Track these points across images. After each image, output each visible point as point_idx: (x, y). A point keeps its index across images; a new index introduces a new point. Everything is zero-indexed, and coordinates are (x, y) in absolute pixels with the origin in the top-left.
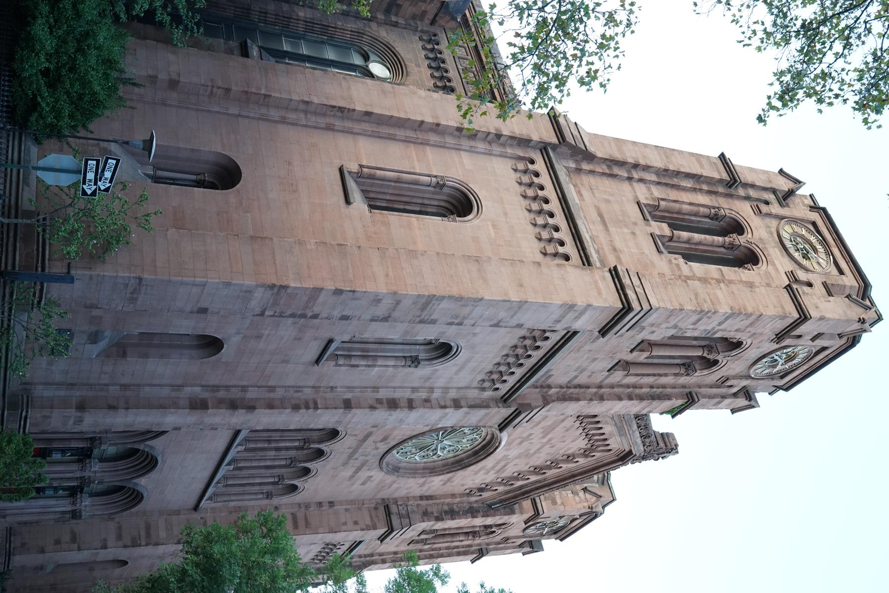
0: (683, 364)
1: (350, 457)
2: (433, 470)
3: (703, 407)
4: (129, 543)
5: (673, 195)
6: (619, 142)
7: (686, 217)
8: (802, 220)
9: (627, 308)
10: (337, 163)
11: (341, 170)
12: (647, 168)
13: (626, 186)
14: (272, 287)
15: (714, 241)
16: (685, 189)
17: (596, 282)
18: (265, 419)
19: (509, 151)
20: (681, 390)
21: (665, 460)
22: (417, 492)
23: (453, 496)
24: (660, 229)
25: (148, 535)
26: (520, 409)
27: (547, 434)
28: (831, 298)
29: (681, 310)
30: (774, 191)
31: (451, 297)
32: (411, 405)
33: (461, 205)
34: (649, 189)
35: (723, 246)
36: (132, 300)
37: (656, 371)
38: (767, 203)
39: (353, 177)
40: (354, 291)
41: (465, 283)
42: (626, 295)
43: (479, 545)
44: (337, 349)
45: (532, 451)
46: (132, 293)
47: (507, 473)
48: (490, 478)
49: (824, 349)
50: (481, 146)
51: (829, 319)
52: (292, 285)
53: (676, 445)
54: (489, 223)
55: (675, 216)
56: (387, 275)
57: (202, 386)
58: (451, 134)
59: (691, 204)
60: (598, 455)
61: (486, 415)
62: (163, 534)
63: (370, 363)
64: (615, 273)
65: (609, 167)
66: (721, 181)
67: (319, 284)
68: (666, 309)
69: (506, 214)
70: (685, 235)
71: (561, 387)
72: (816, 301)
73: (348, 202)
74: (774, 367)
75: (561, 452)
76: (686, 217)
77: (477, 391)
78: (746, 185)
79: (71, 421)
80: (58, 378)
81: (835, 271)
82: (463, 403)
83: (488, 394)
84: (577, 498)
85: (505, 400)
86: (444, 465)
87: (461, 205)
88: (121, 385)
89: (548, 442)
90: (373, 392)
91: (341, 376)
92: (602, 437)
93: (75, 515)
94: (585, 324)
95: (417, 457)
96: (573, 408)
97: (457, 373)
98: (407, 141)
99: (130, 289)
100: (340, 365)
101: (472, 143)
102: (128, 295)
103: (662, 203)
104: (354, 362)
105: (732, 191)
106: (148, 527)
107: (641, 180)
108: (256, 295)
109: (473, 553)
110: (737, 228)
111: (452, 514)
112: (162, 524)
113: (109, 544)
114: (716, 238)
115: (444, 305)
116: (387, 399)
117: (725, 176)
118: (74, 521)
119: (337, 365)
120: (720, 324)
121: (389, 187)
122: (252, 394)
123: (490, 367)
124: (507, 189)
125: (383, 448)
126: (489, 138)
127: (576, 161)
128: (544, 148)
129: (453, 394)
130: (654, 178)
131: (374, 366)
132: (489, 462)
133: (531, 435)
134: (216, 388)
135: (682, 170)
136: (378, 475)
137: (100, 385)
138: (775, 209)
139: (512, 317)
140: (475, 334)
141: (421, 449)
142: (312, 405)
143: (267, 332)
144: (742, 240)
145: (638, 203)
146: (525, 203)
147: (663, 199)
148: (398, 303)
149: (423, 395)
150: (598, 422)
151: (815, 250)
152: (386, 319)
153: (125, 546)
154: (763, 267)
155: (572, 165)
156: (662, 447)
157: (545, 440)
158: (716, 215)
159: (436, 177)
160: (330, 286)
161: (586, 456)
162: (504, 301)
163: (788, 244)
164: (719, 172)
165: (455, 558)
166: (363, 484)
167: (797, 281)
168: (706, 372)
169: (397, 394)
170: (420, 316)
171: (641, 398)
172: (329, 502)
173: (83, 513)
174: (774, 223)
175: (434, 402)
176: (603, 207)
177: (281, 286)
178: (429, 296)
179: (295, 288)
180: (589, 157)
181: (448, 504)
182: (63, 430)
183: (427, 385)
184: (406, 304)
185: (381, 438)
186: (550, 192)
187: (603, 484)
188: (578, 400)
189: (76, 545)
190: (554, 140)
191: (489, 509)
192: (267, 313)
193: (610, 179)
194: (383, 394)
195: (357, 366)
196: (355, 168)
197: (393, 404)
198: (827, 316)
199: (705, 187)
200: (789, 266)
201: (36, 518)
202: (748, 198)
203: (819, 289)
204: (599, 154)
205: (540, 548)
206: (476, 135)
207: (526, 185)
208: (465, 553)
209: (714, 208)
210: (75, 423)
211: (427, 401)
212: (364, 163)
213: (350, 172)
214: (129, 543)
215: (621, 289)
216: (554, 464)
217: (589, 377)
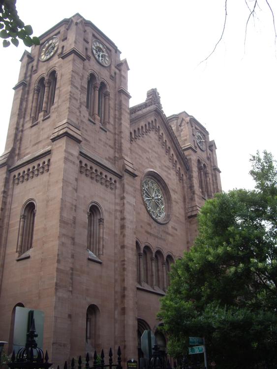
0: (105, 97)
1: (160, 238)
2: (168, 199)
3: (126, 84)
5: (29, 111)
6: (8, 137)
7: (38, 103)
8: (39, 50)
9: (66, 134)
10: (16, 261)
11: (18, 260)
12: (18, 124)
13: (26, 133)
14: (56, 289)
16: (27, 105)
17: (57, 148)
18: (131, 281)
19: (11, 186)
20: (117, 96)
21: (160, 93)
22: (181, 204)
23: (183, 187)
24: (41, 117)
27: (145, 150)
28: (68, 38)
29: (69, 108)
30: (28, 64)
31: (61, 213)
32: (123, 219)
33: (30, 207)
34: (26, 122)
35: (49, 87)
36: (65, 345)
37: (107, 109)
38: (32, 67)
39: (21, 255)
40: (58, 255)
41: (56, 205)
42: (61, 135)
43: (211, 170)
45: (157, 155)
46: (61, 346)
47: (170, 165)
48: (173, 172)
49: (94, 35)
50: (9, 200)
51: (76, 39)
52: (55, 281)
53: (153, 89)
55: (38, 109)
57: (115, 310)
58: (4, 213)
59: (32, 102)
60: (158, 125)
61: (128, 184)
63: (102, 240)
64: (54, 140)
65: (18, 141)
66: (23, 89)
67: (55, 269)
68: (69, 115)
69: (34, 188)
70: (44, 105)
71: (115, 151)
72: (70, 45)
73: (28, 257)
74: (105, 55)
75: (157, 142)
76: (38, 103)
78: (25, 77)
81: (59, 35)
82: (122, 195)
84: (184, 129)
85: (120, 177)
86: (166, 194)
87: (30, 207)
88: (115, 344)
89: (151, 150)
91: (109, 249)
92: (147, 125)
95: (163, 207)
96: (126, 145)
97: (107, 201)
98: (7, 232)
100: (103, 253)
101: (8, 203)
103: (32, 115)
107: (23, 126)
109: (215, 173)
110: (42, 80)
111: (191, 187)
114: (46, 90)
115: (65, 215)
117: (21, 87)
119: (103, 254)
120: (77, 88)
121: (25, 239)
122: (118, 289)
123: (104, 187)
124: (25, 187)
125: (154, 224)
126: (5, 196)
127: (16, 156)
128: (10, 171)
129: (118, 201)
130: (22, 120)
131: (103, 237)
132: (163, 175)
133: (147, 158)
134: (116, 305)
135: (18, 107)
136: (171, 224)
138: (35, 63)
139: (71, 184)
140: (85, 197)
141: (158, 206)
142: (123, 262)
144: (46, 78)
145: (32, 127)
146: (30, 180)
147: (31, 115)
148: (64, 235)
149: (118, 214)
150: (139, 129)
151: (51, 44)
152: (73, 239)
154: (57, 69)
155: (16, 158)
156: (153, 96)
157: (150, 151)
158: (37, 90)
159: (20, 219)
160: (56, 265)
161: (159, 130)
162: (63, 189)
163: (48, 57)
164: (20, 90)
165: (218, 181)
166: (176, 230)
167: (62, 53)
168: (108, 87)
169: (118, 225)
171: (121, 114)
172: (187, 243)
174: (41, 64)
176: (33, 143)
177: (56, 285)
178: (60, 222)
179: (57, 279)
180: (13, 150)
181: (188, 189)
183: (113, 213)
184: (64, 231)
185: (149, 227)
186: (25, 169)
187: (178, 117)
188: (121, 143)
190: (6, 167)
191: (188, 169)
192: (71, 289)
193: (23, 140)
194: (118, 232)
195: (103, 245)
196: (17, 254)
197: (123, 227)
198: (74, 40)
199: (26, 96)
200: (56, 56)
202: (31, 76)
203: (64, 43)
204: (12, 146)
205: (213, 141)
206: (4, 202)
207: (23, 179)
208: (216, 176)
209: (34, 91)
212: (15, 250)
213: (19, 256)
215: (59, 137)
216: (164, 144)
217: (109, 140)
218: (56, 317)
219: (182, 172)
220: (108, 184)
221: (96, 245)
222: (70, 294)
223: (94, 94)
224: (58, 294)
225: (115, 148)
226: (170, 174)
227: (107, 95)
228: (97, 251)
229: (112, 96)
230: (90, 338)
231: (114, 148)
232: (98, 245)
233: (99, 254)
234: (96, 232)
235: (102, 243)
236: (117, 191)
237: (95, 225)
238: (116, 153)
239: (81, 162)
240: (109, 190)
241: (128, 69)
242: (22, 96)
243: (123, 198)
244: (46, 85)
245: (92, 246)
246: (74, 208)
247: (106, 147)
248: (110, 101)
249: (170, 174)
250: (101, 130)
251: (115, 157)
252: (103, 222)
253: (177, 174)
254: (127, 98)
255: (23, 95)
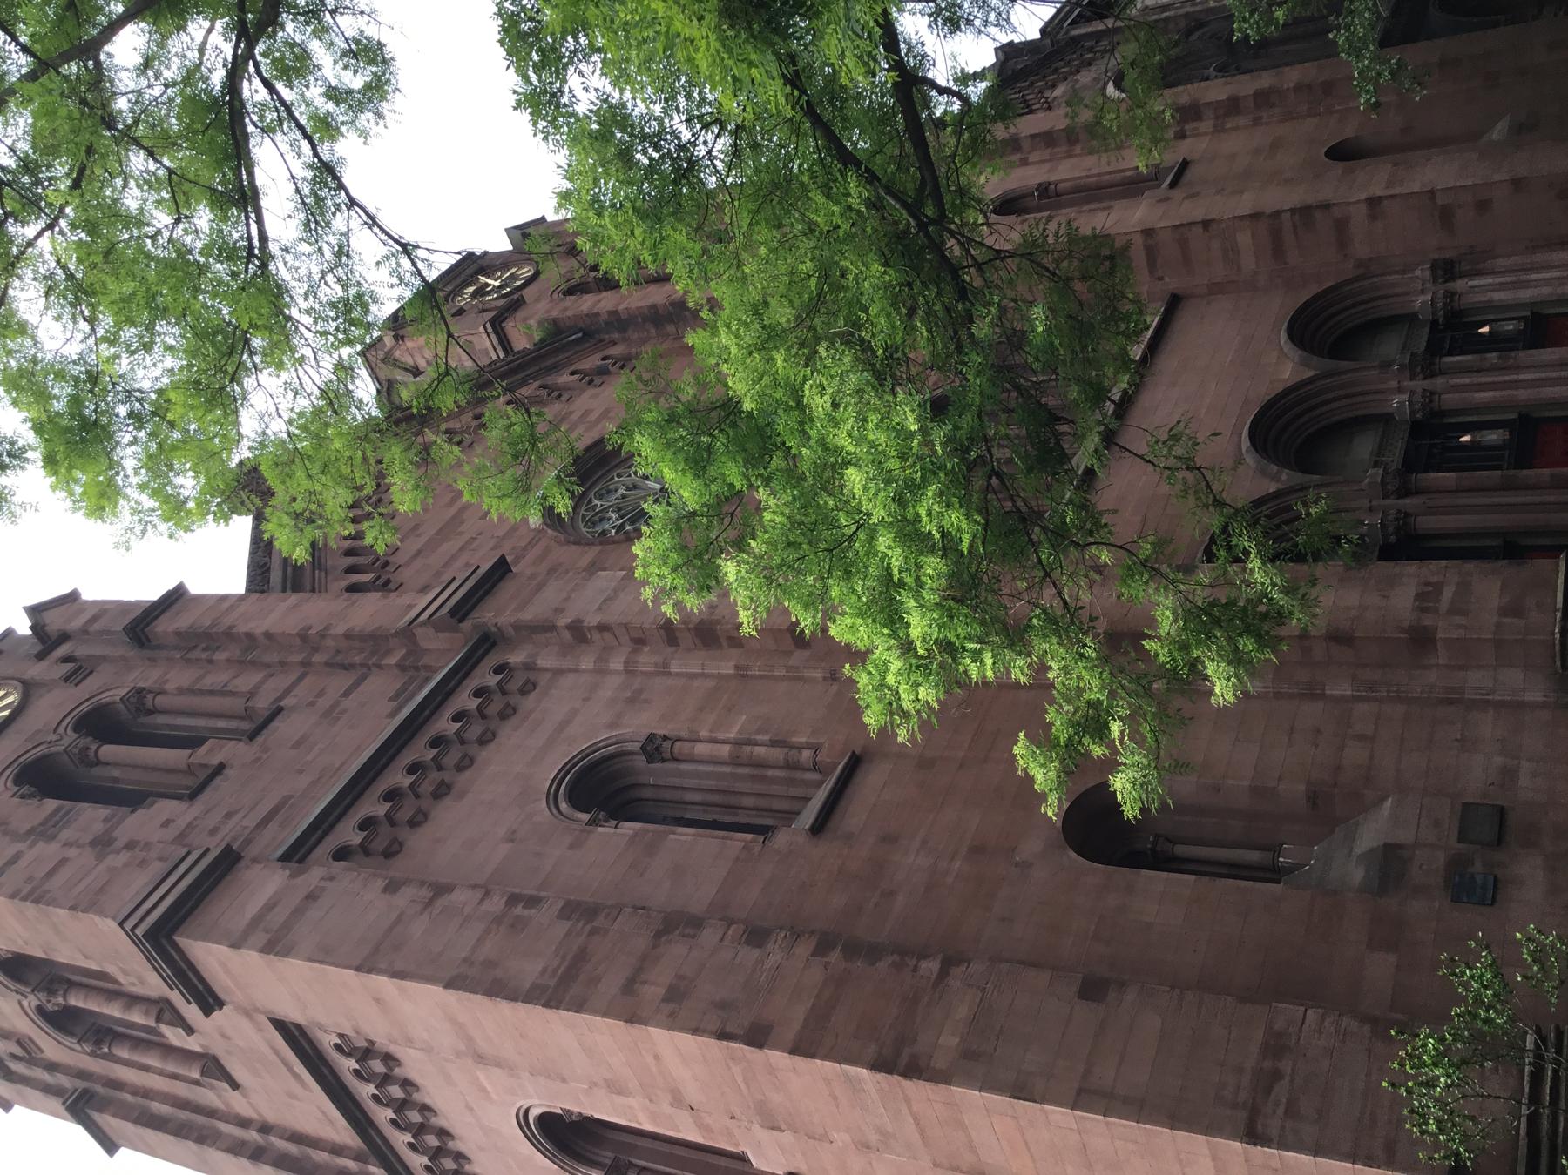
0: (150, 712)
4: (1318, 215)
5: (181, 1090)
15: (86, 998)
25: (1276, 236)
26: (454, 621)
27: (454, 517)
31: (512, 997)
36: (1276, 1046)
44: (819, 784)
46: (1277, 1075)
54: (494, 1097)
56: (657, 1057)
62: (1244, 239)
67: (801, 1062)
71: (379, 667)
77: (541, 663)
79: (1448, 594)
80: (1487, 726)
82: (567, 635)
83: (516, 658)
85: (487, 642)
88: (1323, 696)
90: (747, 668)
93: (1446, 270)
94: (263, 885)
97: (574, 713)
99: (1281, 1090)
100: (808, 746)
102: (1286, 1066)
103: (196, 1075)
104: (778, 754)
105: (81, 1085)
106: (1278, 252)
108: (955, 1041)
112: (1248, 262)
113: (1363, 208)
114: (81, 1004)
116: (720, 646)
118: (1448, 255)
119: (816, 749)
137: (1376, 700)
143: (957, 865)
148: (629, 988)
149: (646, 660)
153: (1325, 206)
158: (98, 1043)
168: (105, 698)
170: (592, 932)
173: (1427, 274)
175: (625, 639)
182: (1470, 566)
184: (611, 984)
188: (348, 636)
189: (1440, 202)
192: (931, 967)
201: (1539, 258)
210: (1439, 587)
211: (639, 642)
214: (1318, 215)
217: (321, 693)
218: (1081, 1091)
219: (592, 362)
220: (501, 706)
221: (773, 781)
222: (957, 971)
223: (116, 765)
224: (940, 1062)
225: (362, 665)
226: (586, 413)
227: (139, 700)
228: (799, 775)
230: (1276, 850)
231: (366, 670)
232: (770, 773)
233: (816, 768)
234: (708, 775)
235: (760, 751)
236: (542, 662)
237: (676, 781)
238: (385, 662)
239: (342, 854)
240: (528, 702)
241: (73, 597)
242: (125, 1118)
243: (579, 632)
244: (60, 1000)
245: (777, 805)
246: (519, 910)
247: (344, 711)
248: (170, 687)
249: (586, 413)
250: (260, 739)
251: (401, 667)
252: (665, 738)
253: (597, 381)
254: (180, 602)
255: (124, 1112)
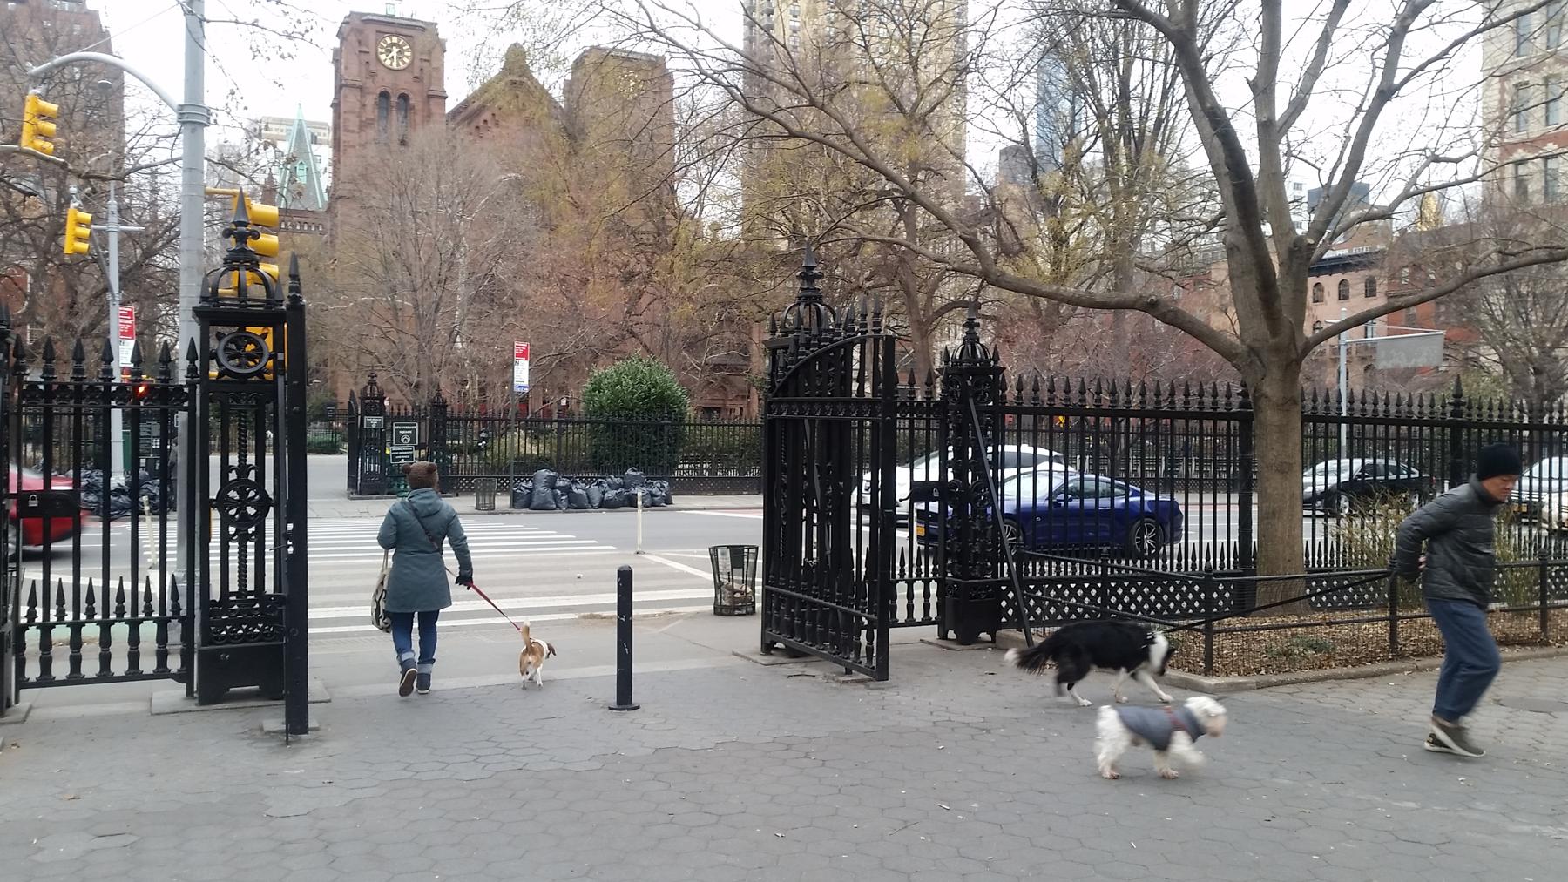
3: (441, 79)
229: (419, 106)
